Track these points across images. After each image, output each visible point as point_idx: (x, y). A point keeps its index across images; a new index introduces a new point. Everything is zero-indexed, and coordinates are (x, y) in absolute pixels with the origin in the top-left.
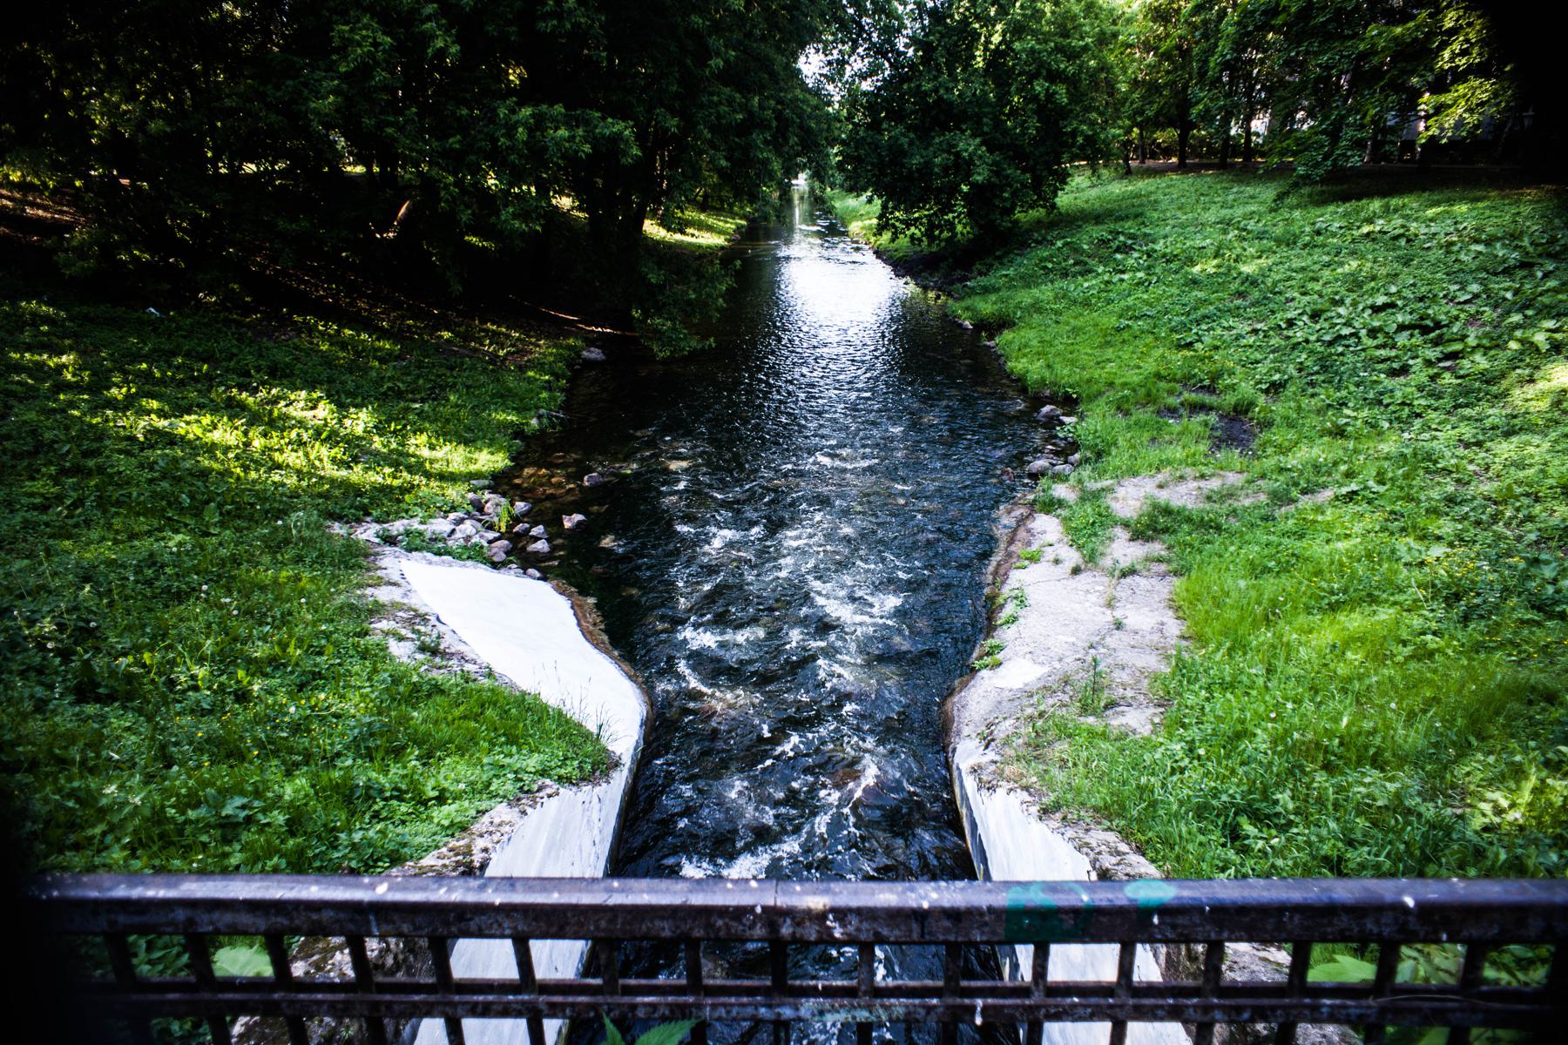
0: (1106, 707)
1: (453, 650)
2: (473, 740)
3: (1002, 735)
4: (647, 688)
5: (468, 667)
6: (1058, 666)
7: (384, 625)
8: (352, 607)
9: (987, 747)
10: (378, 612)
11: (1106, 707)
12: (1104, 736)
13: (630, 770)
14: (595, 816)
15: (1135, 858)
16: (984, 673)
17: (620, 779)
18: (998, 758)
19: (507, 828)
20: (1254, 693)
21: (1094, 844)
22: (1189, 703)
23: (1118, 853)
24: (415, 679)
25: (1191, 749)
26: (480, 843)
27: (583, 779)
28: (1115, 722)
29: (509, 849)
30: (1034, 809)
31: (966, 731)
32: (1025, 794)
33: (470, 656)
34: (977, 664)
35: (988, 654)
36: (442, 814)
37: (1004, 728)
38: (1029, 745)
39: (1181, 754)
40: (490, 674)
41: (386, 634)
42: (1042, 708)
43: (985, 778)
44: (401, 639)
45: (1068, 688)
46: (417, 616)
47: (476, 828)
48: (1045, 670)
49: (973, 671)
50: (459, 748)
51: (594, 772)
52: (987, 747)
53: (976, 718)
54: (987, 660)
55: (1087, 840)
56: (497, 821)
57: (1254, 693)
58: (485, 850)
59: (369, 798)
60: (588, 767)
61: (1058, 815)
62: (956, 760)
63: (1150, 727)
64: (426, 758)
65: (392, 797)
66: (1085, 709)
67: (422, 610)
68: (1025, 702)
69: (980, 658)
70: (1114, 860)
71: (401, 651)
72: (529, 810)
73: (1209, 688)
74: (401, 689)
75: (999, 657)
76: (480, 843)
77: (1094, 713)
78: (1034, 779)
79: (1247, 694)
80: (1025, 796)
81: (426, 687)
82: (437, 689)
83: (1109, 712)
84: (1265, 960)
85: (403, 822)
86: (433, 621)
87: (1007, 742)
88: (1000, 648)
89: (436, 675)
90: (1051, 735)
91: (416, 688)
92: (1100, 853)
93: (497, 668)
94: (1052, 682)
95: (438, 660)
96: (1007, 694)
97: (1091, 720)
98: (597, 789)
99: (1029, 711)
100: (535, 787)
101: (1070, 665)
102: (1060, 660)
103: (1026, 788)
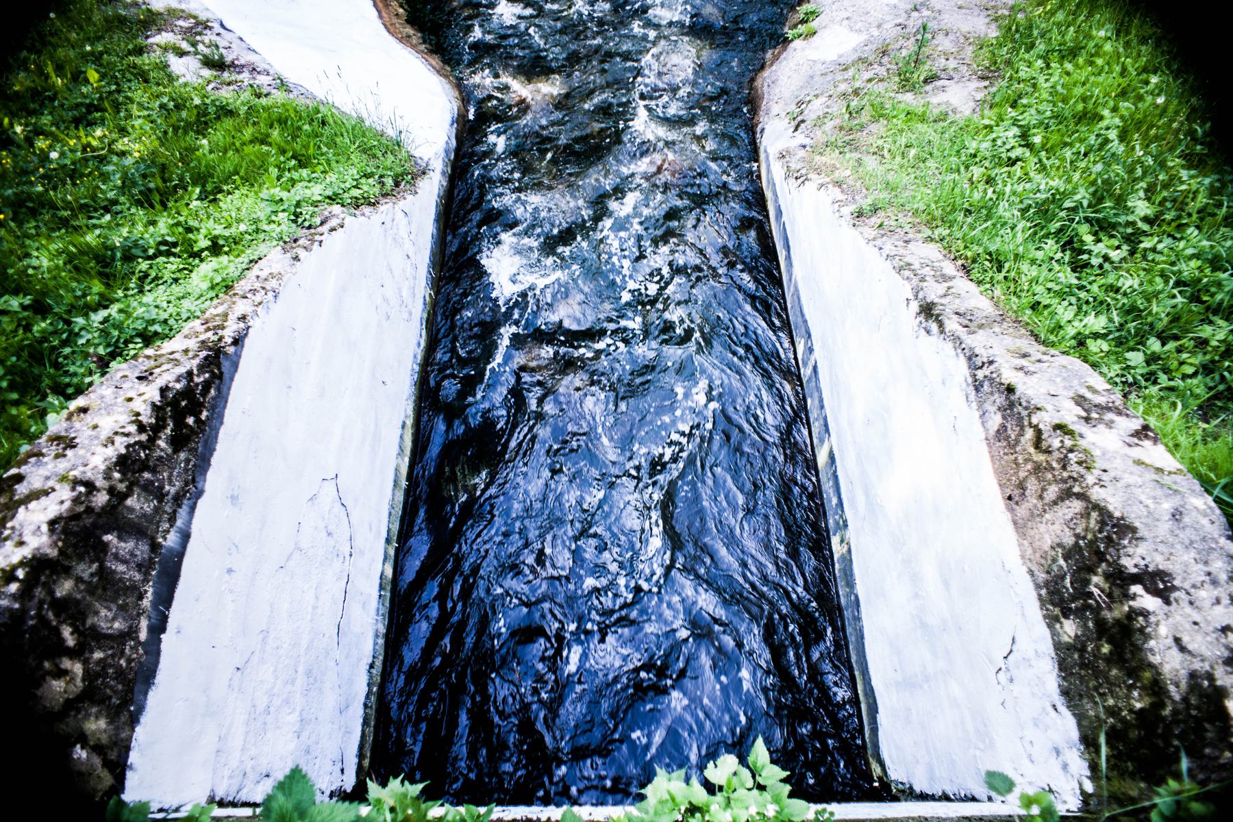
0: (926, 81)
1: (242, 61)
2: (263, 167)
3: (814, 116)
4: (459, 85)
5: (262, 80)
6: (876, 33)
7: (164, 38)
8: (122, 21)
9: (796, 129)
10: (154, 22)
11: (926, 81)
12: (923, 119)
13: (443, 173)
14: (403, 232)
15: (963, 285)
16: (797, 43)
17: (431, 189)
18: (807, 141)
19: (273, 283)
20: (1100, 62)
21: (916, 266)
22: (1022, 74)
23: (946, 278)
24: (197, 101)
25: (1024, 136)
26: (242, 307)
27: (385, 195)
28: (935, 100)
29: (278, 309)
30: (847, 211)
31: (775, 109)
32: (837, 190)
33: (261, 66)
34: (790, 34)
35: (803, 22)
36: (206, 270)
37: (816, 108)
38: (841, 128)
39: (1012, 142)
40: (283, 85)
41: (165, 49)
42: (857, 84)
43: (793, 166)
44: (181, 54)
45: (885, 60)
46: (198, 23)
47: (242, 287)
48: (863, 37)
49: (786, 41)
50: (245, 180)
51: (397, 184)
52: (796, 129)
53: (787, 93)
54: (801, 29)
55: (908, 259)
56: (263, 274)
57: (1100, 62)
58: (243, 318)
59: (128, 257)
60: (389, 182)
61: (875, 220)
62: (764, 144)
63: (972, 104)
64: (211, 196)
65: (159, 253)
66: (906, 84)
67: (203, 16)
68: (839, 77)
69: (795, 26)
70: (941, 288)
71: (186, 70)
72: (302, 254)
73: (1045, 58)
74: (184, 114)
75: (813, 25)
76: (242, 307)
77: (912, 89)
78: (848, 172)
79: (1092, 63)
80: (836, 193)
81: (211, 110)
82: (226, 111)
83: (928, 88)
84: (1139, 463)
85: (176, 280)
86: (216, 26)
87: (820, 121)
88: (814, 14)
89: (226, 94)
90: (865, 117)
91: (202, 111)
92: (923, 280)
93: (291, 77)
94: (868, 53)
95: (226, 74)
96: (819, 68)
97: (909, 97)
98: (402, 203)
99: (843, 87)
100: (318, 220)
101: (890, 31)
102: (879, 26)
103: (838, 184)
